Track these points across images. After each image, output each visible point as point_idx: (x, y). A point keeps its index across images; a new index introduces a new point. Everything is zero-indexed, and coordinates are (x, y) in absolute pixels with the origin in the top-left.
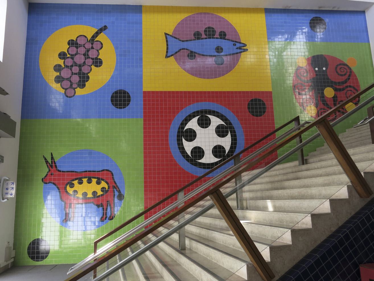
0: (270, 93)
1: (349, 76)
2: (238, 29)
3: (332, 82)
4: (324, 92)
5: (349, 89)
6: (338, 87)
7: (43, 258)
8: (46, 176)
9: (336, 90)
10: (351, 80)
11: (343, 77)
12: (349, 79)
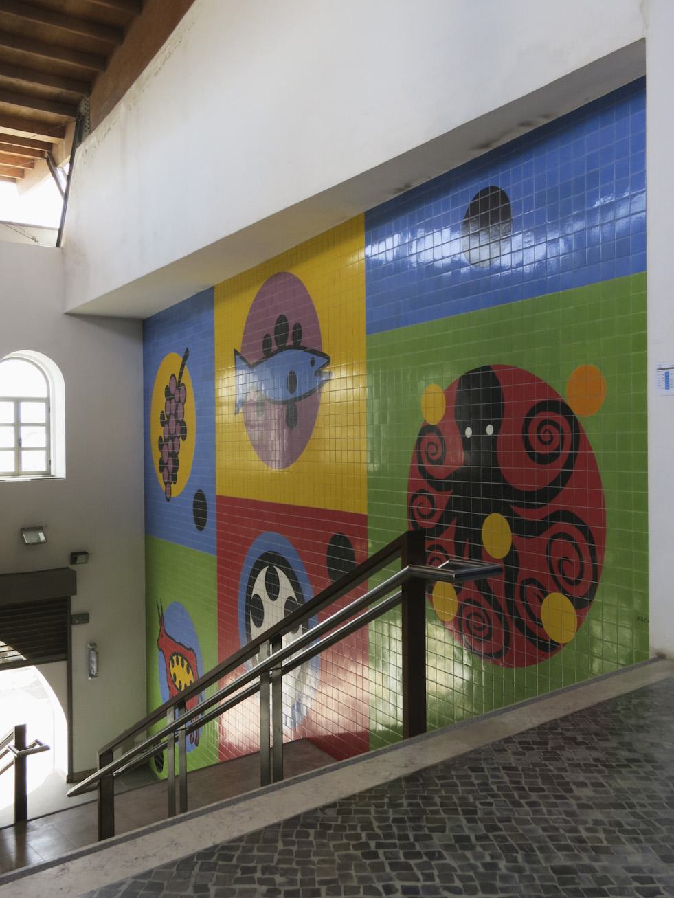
0: (362, 519)
1: (569, 463)
2: (318, 306)
3: (509, 491)
4: (480, 532)
5: (562, 526)
6: (527, 516)
7: (473, 210)
8: (170, 690)
9: (517, 527)
10: (571, 488)
11: (547, 469)
12: (566, 477)
